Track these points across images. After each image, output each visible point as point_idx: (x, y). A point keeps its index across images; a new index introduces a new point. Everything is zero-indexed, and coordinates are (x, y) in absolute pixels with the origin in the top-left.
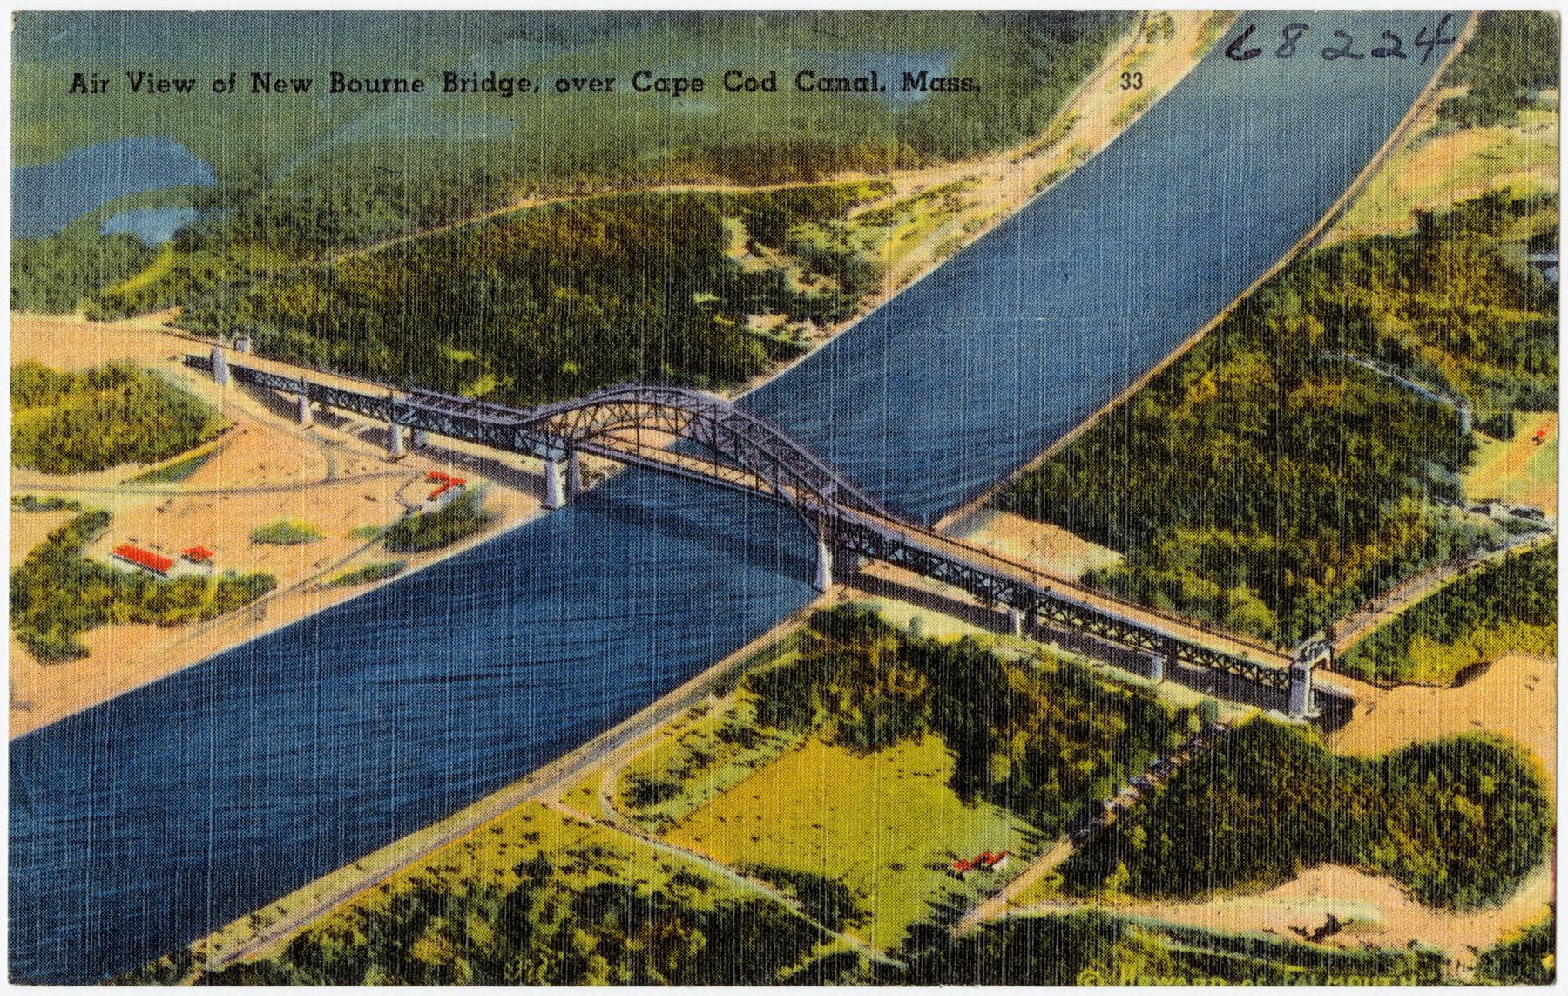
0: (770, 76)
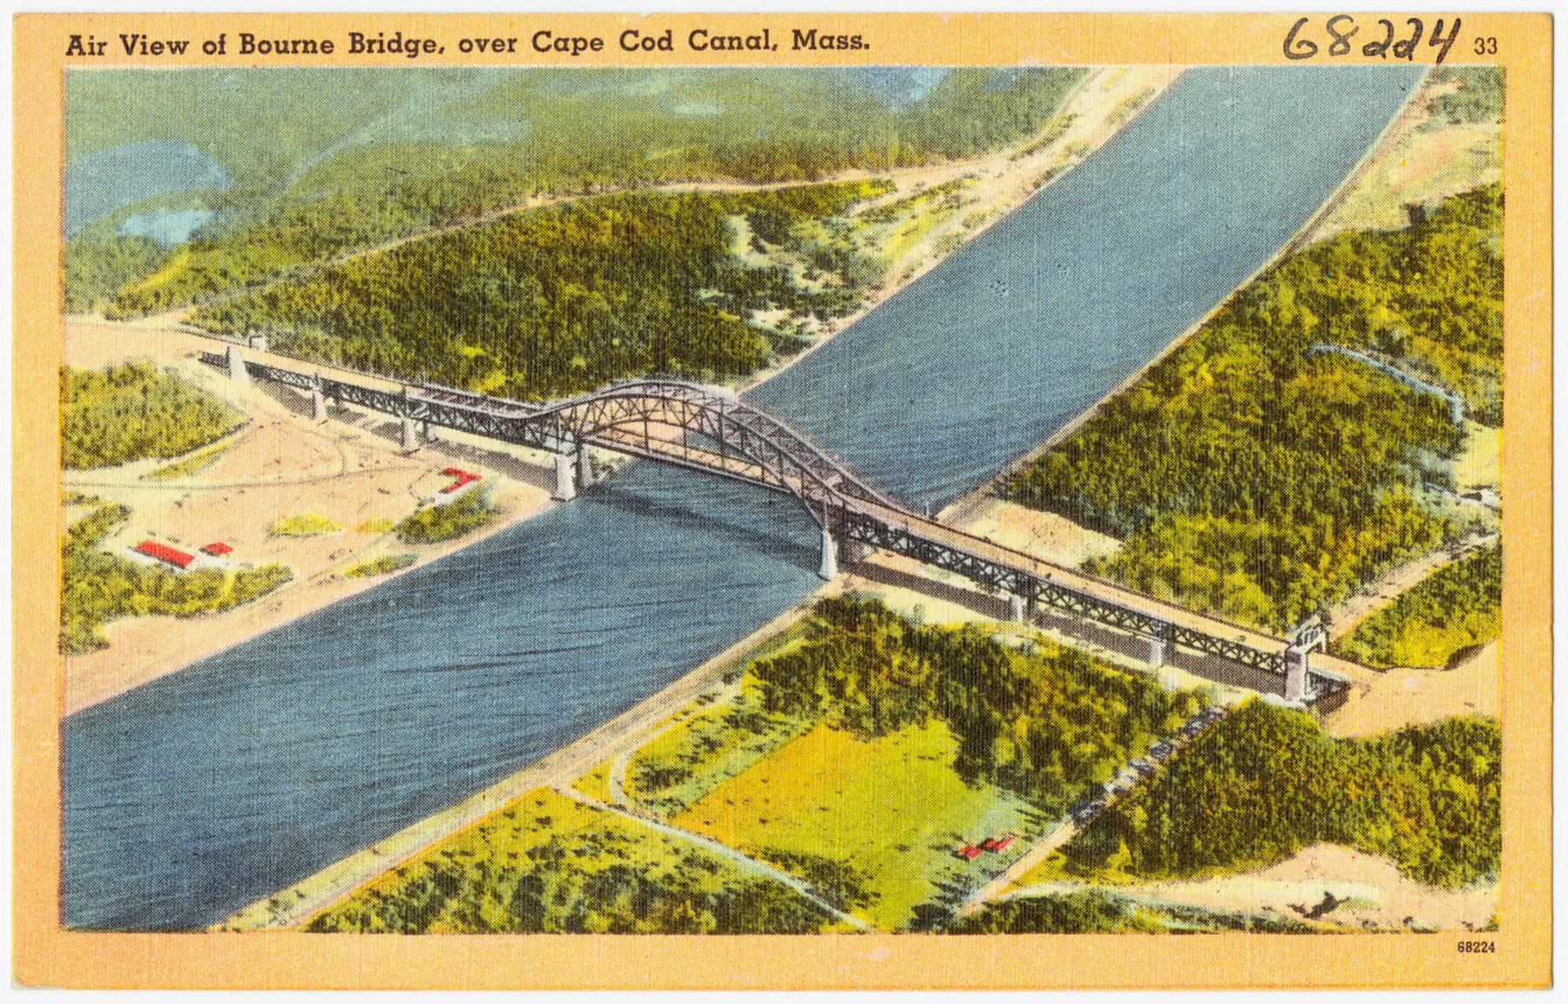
0: (396, 38)
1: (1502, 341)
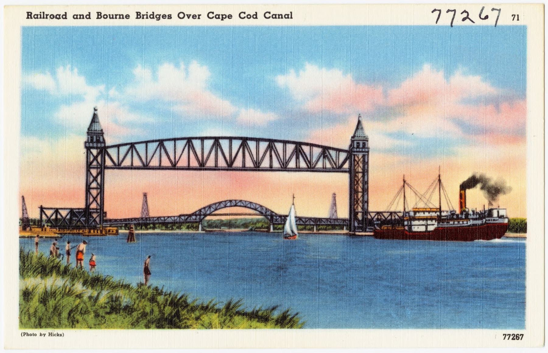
0: (152, 14)
1: (88, 135)
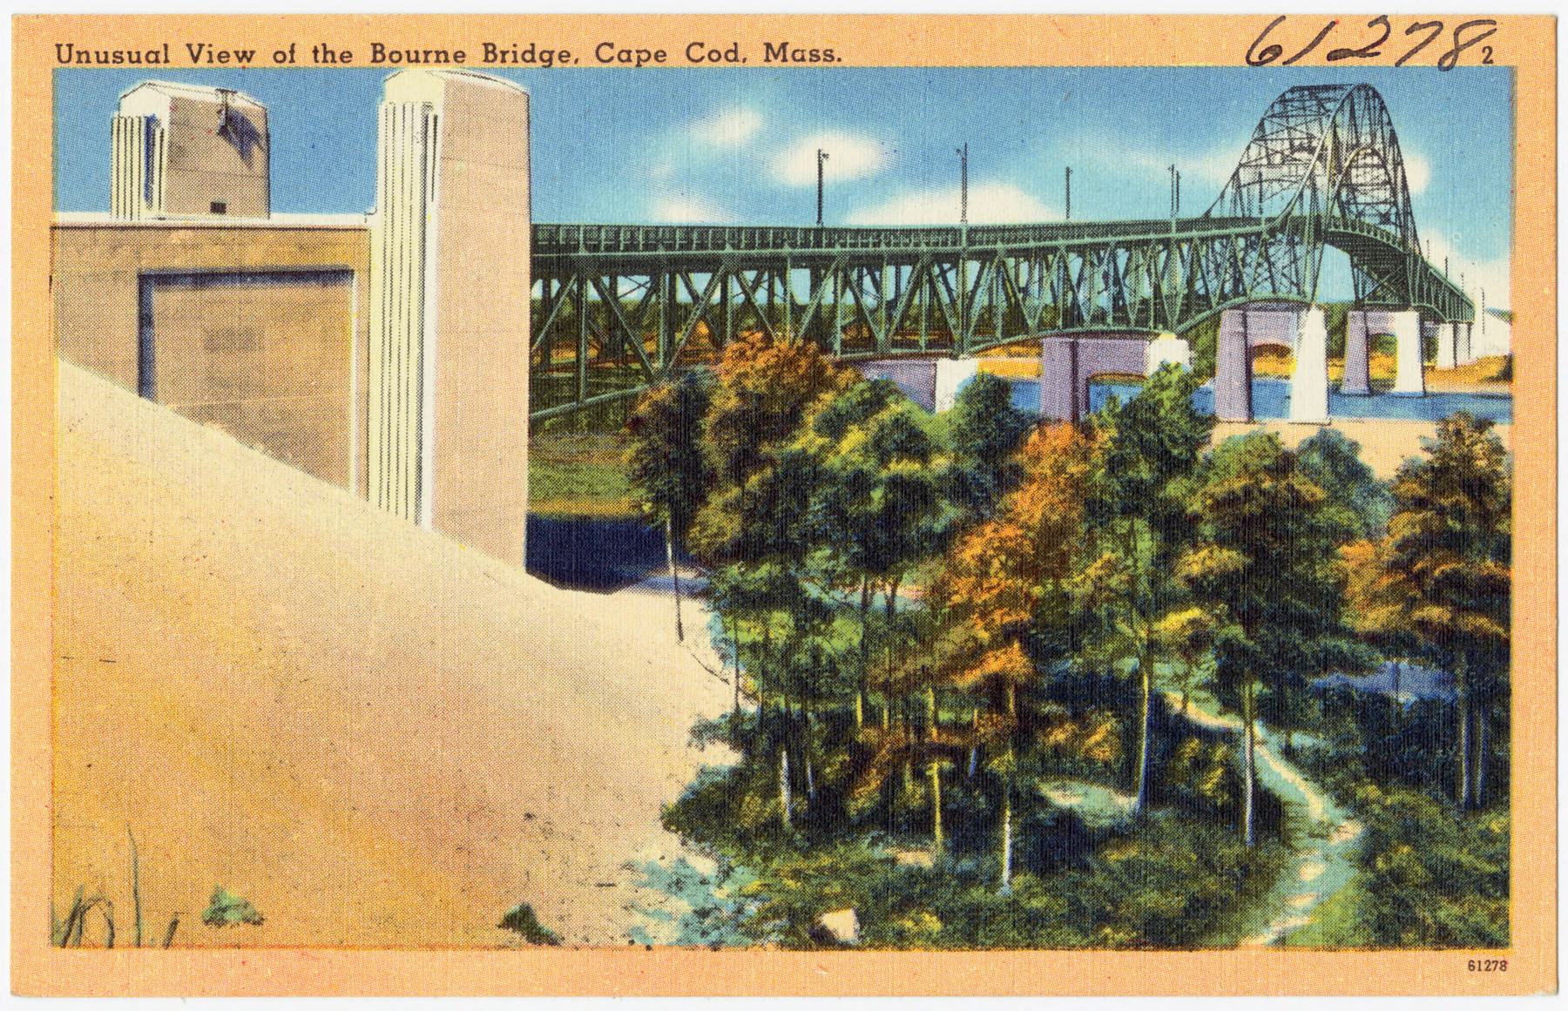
0: (530, 48)
